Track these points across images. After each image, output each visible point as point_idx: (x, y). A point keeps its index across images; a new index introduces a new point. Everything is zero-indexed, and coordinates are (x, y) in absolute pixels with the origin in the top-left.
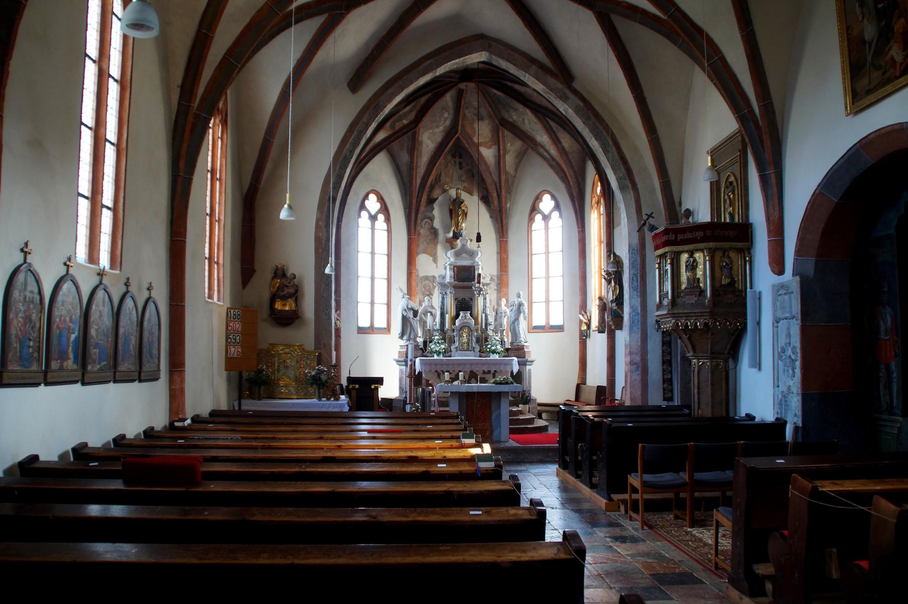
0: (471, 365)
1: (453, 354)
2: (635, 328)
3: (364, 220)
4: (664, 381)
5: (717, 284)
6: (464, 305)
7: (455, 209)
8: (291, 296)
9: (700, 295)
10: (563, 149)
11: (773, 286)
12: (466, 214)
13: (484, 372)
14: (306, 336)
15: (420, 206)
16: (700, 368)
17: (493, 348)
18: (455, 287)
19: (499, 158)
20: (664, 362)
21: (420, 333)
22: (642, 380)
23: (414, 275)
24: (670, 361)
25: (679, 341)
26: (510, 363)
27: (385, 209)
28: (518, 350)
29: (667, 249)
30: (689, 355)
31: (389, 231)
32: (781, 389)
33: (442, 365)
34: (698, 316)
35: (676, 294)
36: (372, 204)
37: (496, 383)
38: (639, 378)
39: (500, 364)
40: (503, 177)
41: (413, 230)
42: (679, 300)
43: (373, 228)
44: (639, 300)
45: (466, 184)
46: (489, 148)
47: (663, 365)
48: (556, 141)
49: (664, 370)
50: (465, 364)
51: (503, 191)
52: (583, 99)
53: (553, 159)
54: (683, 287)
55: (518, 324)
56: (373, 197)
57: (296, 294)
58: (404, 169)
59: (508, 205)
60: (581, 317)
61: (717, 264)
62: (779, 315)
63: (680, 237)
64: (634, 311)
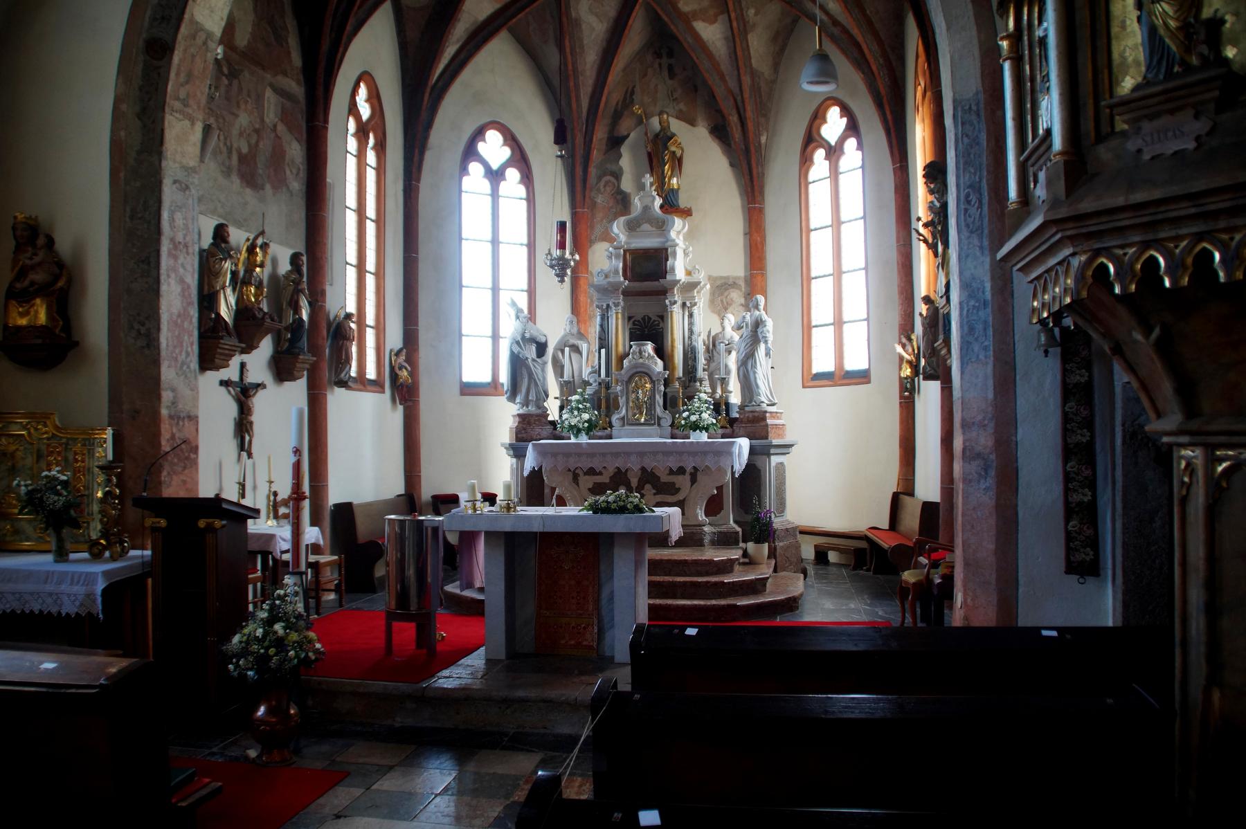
0: (641, 454)
1: (615, 432)
2: (976, 348)
3: (475, 177)
4: (1069, 512)
6: (650, 329)
7: (660, 155)
8: (42, 290)
12: (680, 160)
13: (671, 472)
14: (88, 389)
15: (593, 148)
16: (1218, 490)
17: (693, 418)
18: (626, 293)
19: (737, 37)
21: (554, 389)
23: (582, 282)
26: (726, 451)
27: (520, 159)
28: (752, 422)
31: (531, 199)
33: (579, 455)
35: (1088, 125)
36: (494, 148)
37: (596, 509)
39: (705, 453)
40: (747, 80)
41: (579, 196)
42: (1104, 153)
43: (495, 195)
45: (682, 106)
46: (712, 21)
49: (1067, 478)
50: (628, 454)
51: (749, 108)
54: (1127, 84)
55: (754, 366)
56: (834, 113)
57: (61, 284)
58: (556, 81)
59: (763, 139)
60: (899, 349)
64: (970, 296)
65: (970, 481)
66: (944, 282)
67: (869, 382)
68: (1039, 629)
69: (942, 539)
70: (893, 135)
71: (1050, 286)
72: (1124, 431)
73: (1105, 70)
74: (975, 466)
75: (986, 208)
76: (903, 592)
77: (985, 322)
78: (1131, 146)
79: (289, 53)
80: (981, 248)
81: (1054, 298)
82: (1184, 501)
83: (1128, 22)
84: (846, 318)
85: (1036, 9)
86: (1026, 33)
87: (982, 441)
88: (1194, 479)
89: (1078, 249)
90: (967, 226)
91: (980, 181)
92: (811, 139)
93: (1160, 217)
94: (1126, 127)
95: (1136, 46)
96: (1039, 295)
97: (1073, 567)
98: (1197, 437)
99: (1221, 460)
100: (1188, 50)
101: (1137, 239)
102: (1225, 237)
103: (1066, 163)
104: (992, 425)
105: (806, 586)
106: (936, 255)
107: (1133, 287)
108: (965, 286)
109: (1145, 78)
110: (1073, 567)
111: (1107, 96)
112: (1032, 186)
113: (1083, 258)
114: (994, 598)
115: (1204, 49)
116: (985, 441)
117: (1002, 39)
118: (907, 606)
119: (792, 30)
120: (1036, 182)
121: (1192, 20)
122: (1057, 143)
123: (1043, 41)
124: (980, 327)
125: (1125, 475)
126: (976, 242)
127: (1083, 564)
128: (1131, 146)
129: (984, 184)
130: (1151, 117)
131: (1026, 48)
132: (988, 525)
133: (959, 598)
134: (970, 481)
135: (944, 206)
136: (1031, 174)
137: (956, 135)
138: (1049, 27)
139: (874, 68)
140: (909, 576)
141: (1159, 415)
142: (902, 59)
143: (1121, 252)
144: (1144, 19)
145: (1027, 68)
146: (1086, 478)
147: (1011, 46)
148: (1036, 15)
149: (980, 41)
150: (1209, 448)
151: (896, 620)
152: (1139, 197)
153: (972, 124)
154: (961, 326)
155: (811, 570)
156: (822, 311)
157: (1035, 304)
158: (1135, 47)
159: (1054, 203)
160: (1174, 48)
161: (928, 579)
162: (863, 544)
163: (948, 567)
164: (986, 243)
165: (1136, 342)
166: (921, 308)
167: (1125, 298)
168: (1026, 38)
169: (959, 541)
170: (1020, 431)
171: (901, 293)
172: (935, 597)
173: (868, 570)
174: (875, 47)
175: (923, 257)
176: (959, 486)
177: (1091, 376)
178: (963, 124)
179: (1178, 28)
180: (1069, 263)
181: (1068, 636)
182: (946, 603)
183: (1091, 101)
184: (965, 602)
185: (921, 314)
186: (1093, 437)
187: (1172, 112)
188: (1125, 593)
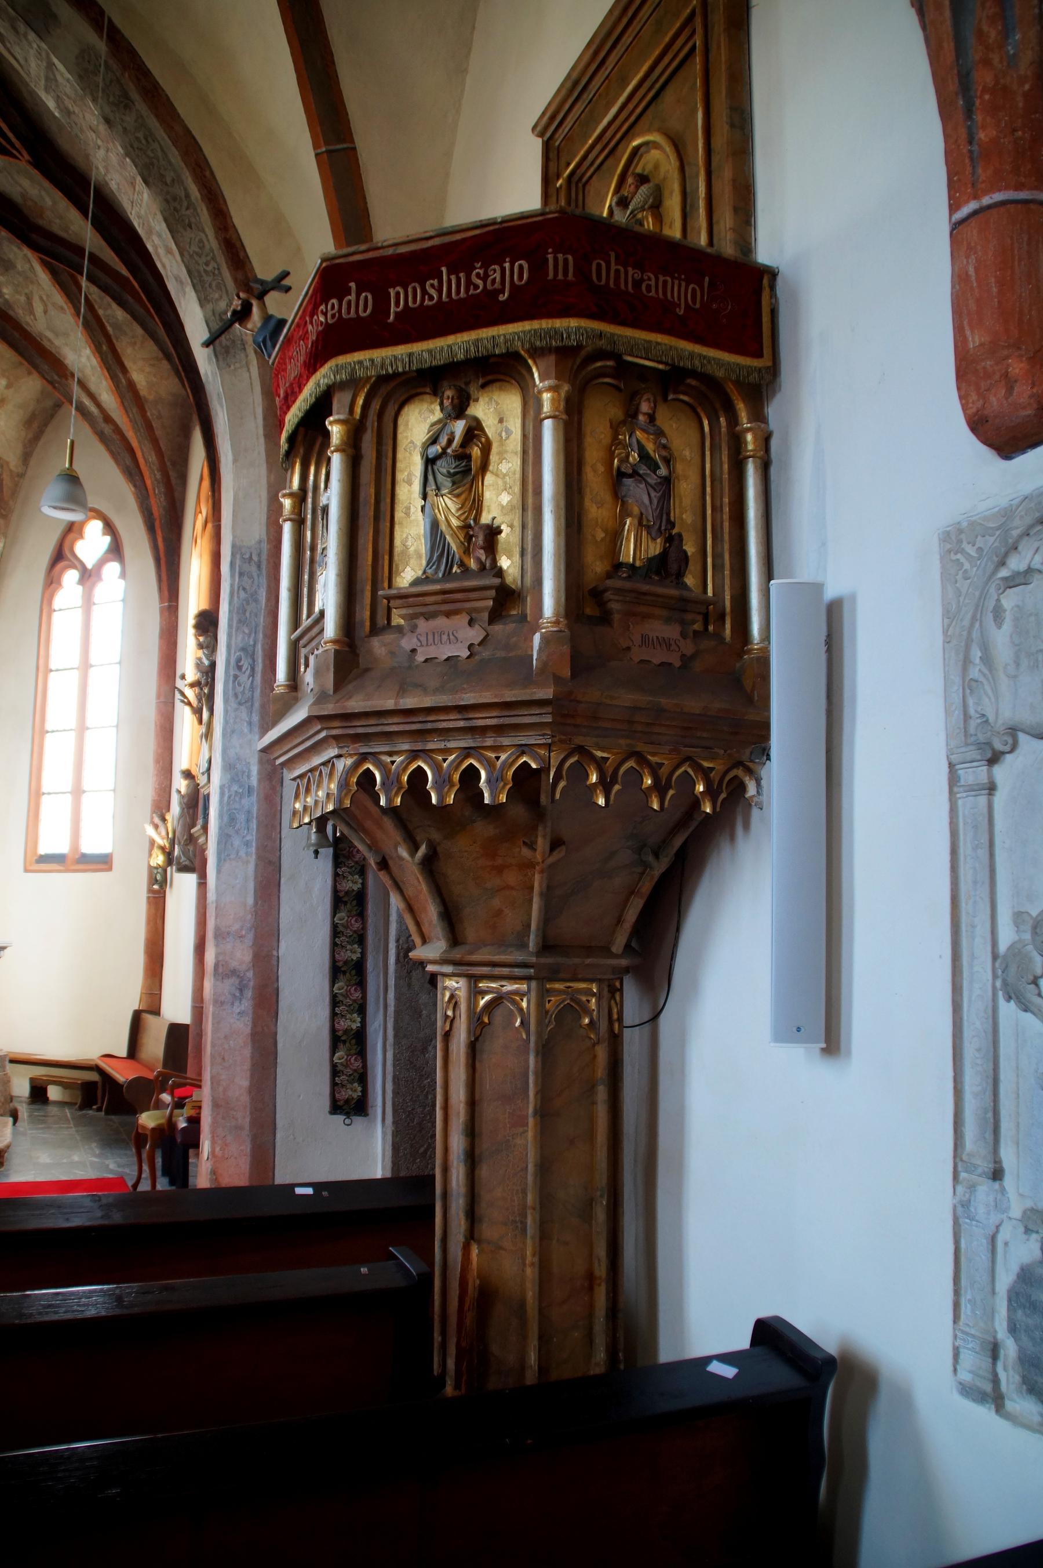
2: (237, 842)
4: (336, 1040)
5: (596, 566)
9: (496, 615)
10: (131, 385)
20: (336, 971)
22: (252, 1034)
24: (359, 968)
25: (395, 901)
29: (323, 377)
30: (431, 951)
32: (1018, 1193)
34: (481, 725)
35: (364, 614)
42: (378, 646)
48: (113, 361)
52: (115, 38)
53: (108, 419)
54: (407, 576)
56: (94, 528)
60: (150, 831)
61: (593, 454)
62: (1009, 703)
63: (400, 299)
65: (222, 1003)
66: (207, 757)
67: (110, 869)
68: (292, 1186)
69: (191, 1073)
71: (313, 788)
72: (397, 947)
73: (385, 556)
74: (229, 986)
76: (139, 1139)
77: (249, 812)
78: (407, 643)
80: (250, 723)
81: (316, 802)
82: (447, 1035)
83: (412, 510)
84: (69, 798)
85: (324, 471)
86: (310, 494)
88: (457, 1013)
89: (344, 751)
90: (236, 695)
91: (254, 645)
92: (61, 556)
93: (429, 726)
94: (402, 622)
95: (419, 536)
96: (302, 796)
97: (337, 1107)
98: (461, 966)
99: (484, 993)
100: (467, 551)
101: (406, 747)
102: (388, 759)
103: (336, 651)
104: (251, 936)
105: (15, 1134)
106: (200, 722)
107: (399, 800)
108: (229, 766)
109: (424, 572)
110: (337, 1107)
111: (386, 585)
112: (302, 669)
113: (349, 761)
114: (247, 1147)
115: (482, 554)
116: (242, 955)
117: (284, 496)
118: (144, 1156)
119: (52, 416)
120: (307, 665)
121: (472, 522)
122: (330, 628)
123: (325, 510)
124: (242, 817)
125: (397, 999)
126: (244, 715)
127: (348, 1103)
129: (259, 647)
130: (429, 616)
131: (309, 511)
132: (242, 1056)
133: (206, 1146)
134: (222, 1003)
135: (213, 665)
136: (302, 656)
137: (232, 586)
138: (333, 497)
139: (148, 482)
140: (148, 1120)
141: (424, 941)
142: (183, 478)
143: (389, 759)
144: (427, 509)
145: (309, 534)
146: (355, 1001)
147: (294, 507)
148: (323, 477)
149: (269, 483)
150: (473, 979)
151: (130, 1174)
153: (251, 577)
154: (221, 816)
155: (23, 1111)
156: (56, 774)
157: (297, 805)
158: (417, 538)
159: (321, 698)
160: (454, 547)
161: (171, 1123)
162: (94, 1076)
163: (194, 1107)
164: (256, 718)
165: (401, 859)
166: (180, 784)
167: (391, 811)
168: (310, 500)
169: (207, 1077)
170: (283, 945)
171: (157, 761)
172: (176, 1147)
173: (99, 1109)
174: (153, 458)
175: (186, 722)
176: (209, 1009)
177: (364, 885)
178: (241, 574)
179: (458, 527)
180: (333, 764)
181: (325, 1194)
182: (191, 1152)
183: (369, 588)
184: (213, 1152)
185: (179, 792)
186: (363, 954)
187: (448, 614)
188: (395, 1134)
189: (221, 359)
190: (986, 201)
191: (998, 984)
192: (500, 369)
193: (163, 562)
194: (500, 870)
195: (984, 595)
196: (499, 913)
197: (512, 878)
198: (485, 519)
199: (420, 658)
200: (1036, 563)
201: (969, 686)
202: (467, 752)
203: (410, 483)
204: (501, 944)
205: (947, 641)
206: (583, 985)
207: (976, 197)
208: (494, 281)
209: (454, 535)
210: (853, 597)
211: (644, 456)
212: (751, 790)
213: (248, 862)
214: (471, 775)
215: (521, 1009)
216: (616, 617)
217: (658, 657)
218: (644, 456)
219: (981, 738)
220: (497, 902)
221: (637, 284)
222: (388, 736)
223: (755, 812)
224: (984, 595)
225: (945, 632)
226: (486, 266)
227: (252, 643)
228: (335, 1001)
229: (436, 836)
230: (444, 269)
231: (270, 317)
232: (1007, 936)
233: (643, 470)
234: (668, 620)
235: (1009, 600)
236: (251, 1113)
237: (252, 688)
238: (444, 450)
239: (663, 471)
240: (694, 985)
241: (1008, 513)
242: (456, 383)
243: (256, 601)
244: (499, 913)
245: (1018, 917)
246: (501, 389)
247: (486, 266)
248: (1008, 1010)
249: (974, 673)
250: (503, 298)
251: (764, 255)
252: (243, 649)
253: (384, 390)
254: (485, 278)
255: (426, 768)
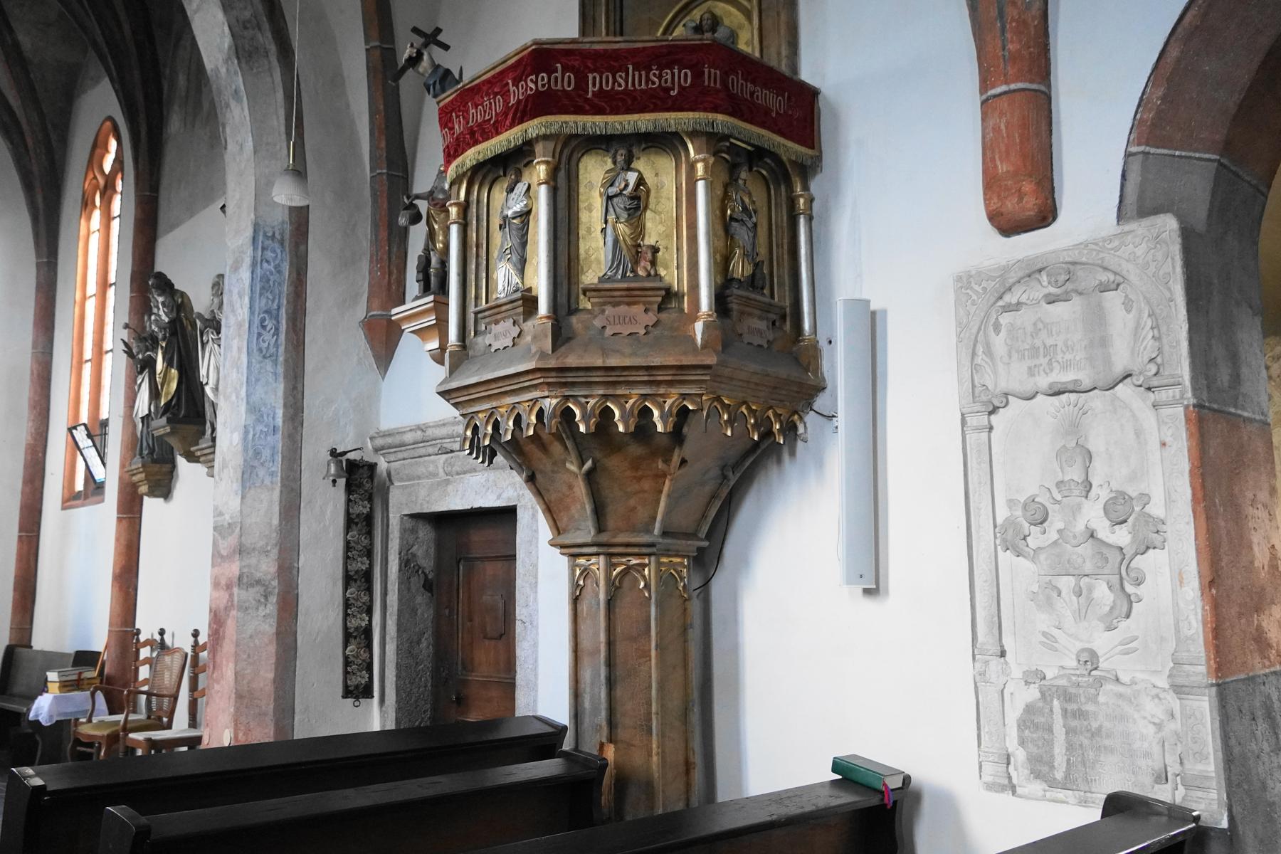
2: (262, 472)
4: (348, 636)
11: (965, 282)
20: (348, 579)
22: (278, 633)
24: (368, 576)
29: (533, 127)
32: (1017, 663)
38: (269, 628)
44: (280, 388)
47: (346, 586)
62: (1011, 376)
63: (596, 83)
65: (247, 609)
70: (41, 218)
75: (282, 337)
79: (107, 43)
80: (275, 374)
87: (264, 567)
90: (260, 350)
97: (348, 693)
102: (583, 400)
110: (348, 693)
116: (267, 567)
124: (266, 453)
128: (598, 323)
129: (283, 312)
130: (615, 305)
152: (613, 362)
170: (302, 557)
178: (263, 249)
186: (371, 565)
187: (629, 304)
189: (243, 61)
190: (1013, 86)
191: (998, 542)
192: (665, 142)
193: (41, 218)
194: (639, 479)
195: (987, 315)
196: (633, 509)
197: (647, 485)
198: (650, 240)
199: (608, 332)
200: (1023, 299)
201: (975, 368)
202: (606, 397)
203: (590, 209)
204: (633, 529)
205: (960, 341)
206: (678, 560)
207: (1007, 83)
208: (666, 81)
209: (629, 249)
210: (885, 312)
211: (745, 209)
212: (801, 430)
213: (273, 489)
214: (646, 412)
215: (644, 577)
216: (735, 314)
217: (757, 341)
218: (745, 209)
219: (984, 398)
220: (632, 502)
221: (752, 94)
222: (589, 384)
223: (800, 444)
224: (987, 315)
225: (958, 336)
226: (661, 69)
227: (275, 306)
228: (347, 604)
229: (598, 455)
230: (630, 67)
231: (439, 66)
232: (1002, 514)
233: (745, 218)
234: (760, 318)
235: (1005, 319)
236: (275, 700)
237: (277, 345)
238: (621, 191)
239: (754, 219)
240: (744, 561)
241: (1006, 269)
242: (627, 146)
243: (279, 272)
244: (633, 509)
245: (1011, 503)
246: (656, 153)
247: (661, 69)
248: (1006, 557)
249: (978, 360)
250: (672, 93)
251: (807, 74)
252: (266, 312)
253: (574, 143)
254: (660, 77)
255: (612, 407)
